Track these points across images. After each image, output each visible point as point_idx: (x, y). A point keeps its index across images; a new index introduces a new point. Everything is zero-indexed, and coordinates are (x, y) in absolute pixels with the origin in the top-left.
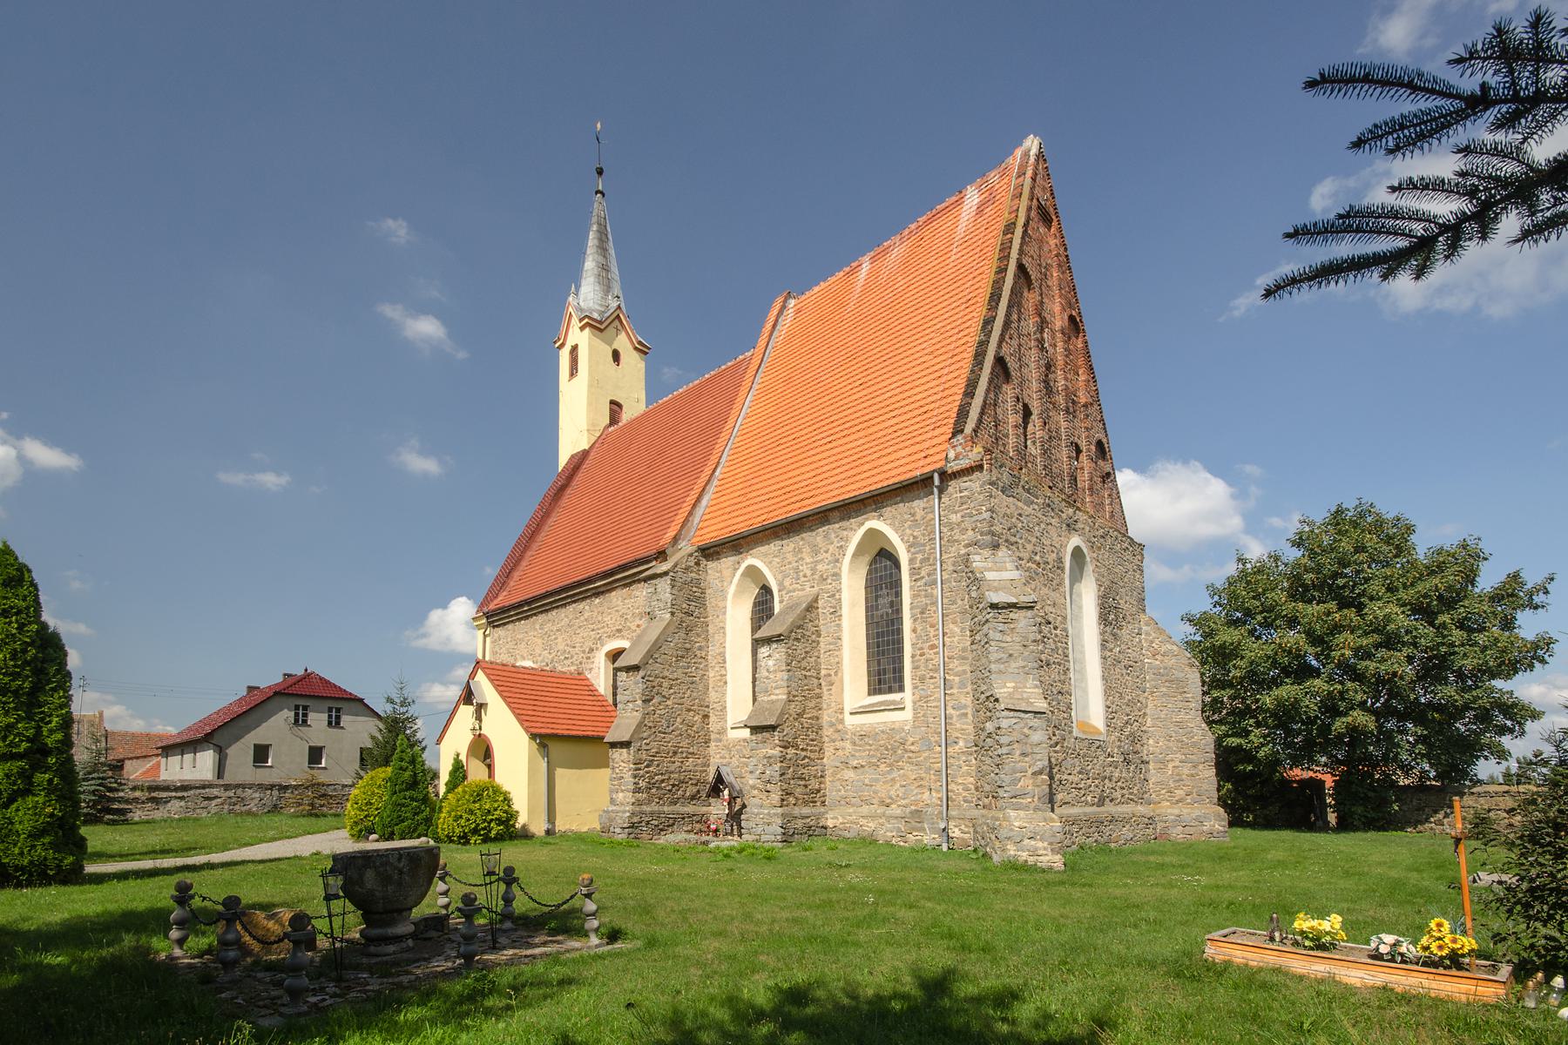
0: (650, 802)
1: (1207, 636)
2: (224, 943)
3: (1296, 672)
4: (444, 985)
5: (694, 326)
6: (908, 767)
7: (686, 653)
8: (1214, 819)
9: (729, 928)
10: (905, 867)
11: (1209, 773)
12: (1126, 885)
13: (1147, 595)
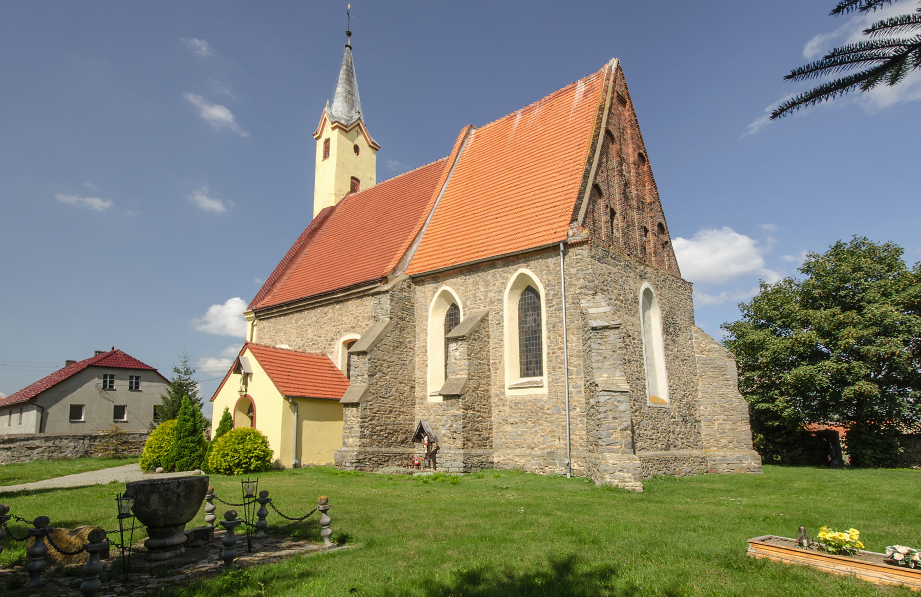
0: (372, 445)
1: (739, 337)
2: (32, 555)
3: (810, 357)
4: (207, 582)
5: (410, 135)
6: (545, 424)
7: (399, 345)
8: (751, 460)
9: (426, 532)
10: (544, 489)
11: (745, 428)
12: (687, 503)
13: (695, 313)
